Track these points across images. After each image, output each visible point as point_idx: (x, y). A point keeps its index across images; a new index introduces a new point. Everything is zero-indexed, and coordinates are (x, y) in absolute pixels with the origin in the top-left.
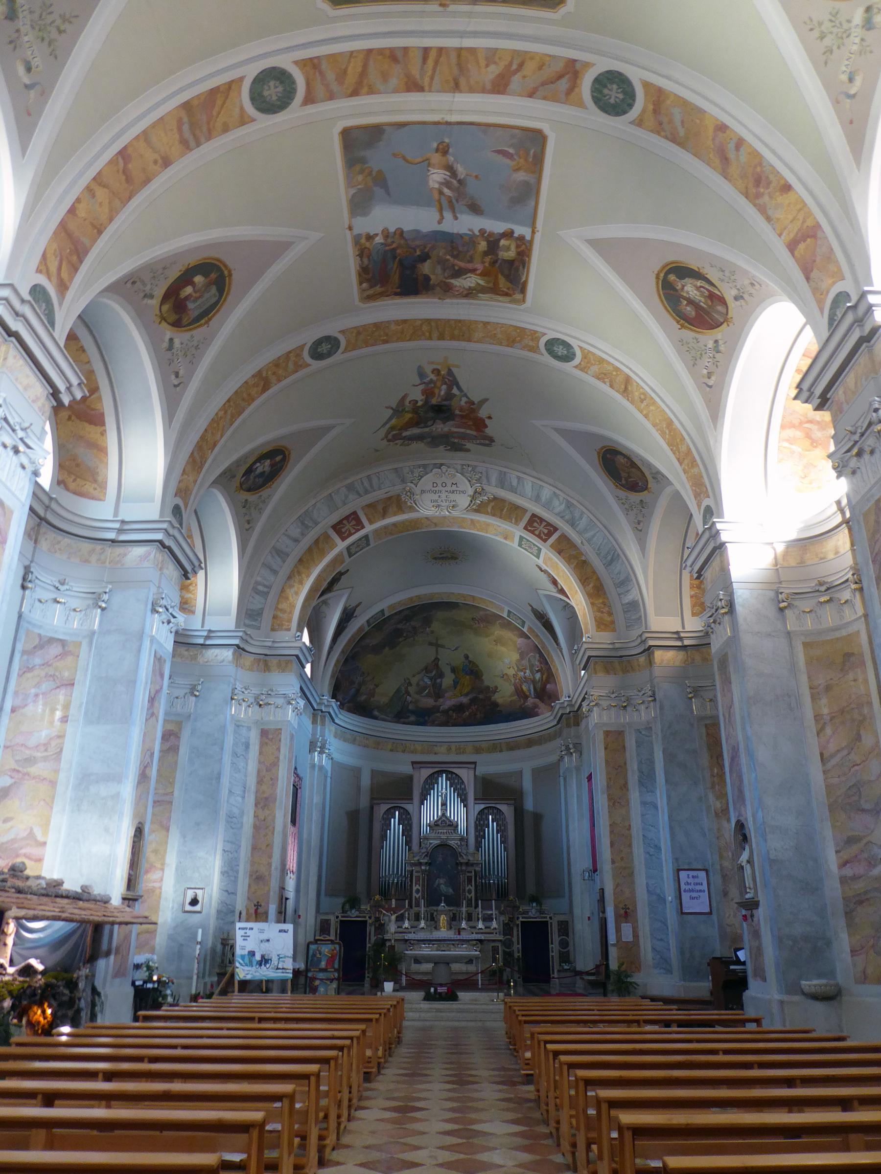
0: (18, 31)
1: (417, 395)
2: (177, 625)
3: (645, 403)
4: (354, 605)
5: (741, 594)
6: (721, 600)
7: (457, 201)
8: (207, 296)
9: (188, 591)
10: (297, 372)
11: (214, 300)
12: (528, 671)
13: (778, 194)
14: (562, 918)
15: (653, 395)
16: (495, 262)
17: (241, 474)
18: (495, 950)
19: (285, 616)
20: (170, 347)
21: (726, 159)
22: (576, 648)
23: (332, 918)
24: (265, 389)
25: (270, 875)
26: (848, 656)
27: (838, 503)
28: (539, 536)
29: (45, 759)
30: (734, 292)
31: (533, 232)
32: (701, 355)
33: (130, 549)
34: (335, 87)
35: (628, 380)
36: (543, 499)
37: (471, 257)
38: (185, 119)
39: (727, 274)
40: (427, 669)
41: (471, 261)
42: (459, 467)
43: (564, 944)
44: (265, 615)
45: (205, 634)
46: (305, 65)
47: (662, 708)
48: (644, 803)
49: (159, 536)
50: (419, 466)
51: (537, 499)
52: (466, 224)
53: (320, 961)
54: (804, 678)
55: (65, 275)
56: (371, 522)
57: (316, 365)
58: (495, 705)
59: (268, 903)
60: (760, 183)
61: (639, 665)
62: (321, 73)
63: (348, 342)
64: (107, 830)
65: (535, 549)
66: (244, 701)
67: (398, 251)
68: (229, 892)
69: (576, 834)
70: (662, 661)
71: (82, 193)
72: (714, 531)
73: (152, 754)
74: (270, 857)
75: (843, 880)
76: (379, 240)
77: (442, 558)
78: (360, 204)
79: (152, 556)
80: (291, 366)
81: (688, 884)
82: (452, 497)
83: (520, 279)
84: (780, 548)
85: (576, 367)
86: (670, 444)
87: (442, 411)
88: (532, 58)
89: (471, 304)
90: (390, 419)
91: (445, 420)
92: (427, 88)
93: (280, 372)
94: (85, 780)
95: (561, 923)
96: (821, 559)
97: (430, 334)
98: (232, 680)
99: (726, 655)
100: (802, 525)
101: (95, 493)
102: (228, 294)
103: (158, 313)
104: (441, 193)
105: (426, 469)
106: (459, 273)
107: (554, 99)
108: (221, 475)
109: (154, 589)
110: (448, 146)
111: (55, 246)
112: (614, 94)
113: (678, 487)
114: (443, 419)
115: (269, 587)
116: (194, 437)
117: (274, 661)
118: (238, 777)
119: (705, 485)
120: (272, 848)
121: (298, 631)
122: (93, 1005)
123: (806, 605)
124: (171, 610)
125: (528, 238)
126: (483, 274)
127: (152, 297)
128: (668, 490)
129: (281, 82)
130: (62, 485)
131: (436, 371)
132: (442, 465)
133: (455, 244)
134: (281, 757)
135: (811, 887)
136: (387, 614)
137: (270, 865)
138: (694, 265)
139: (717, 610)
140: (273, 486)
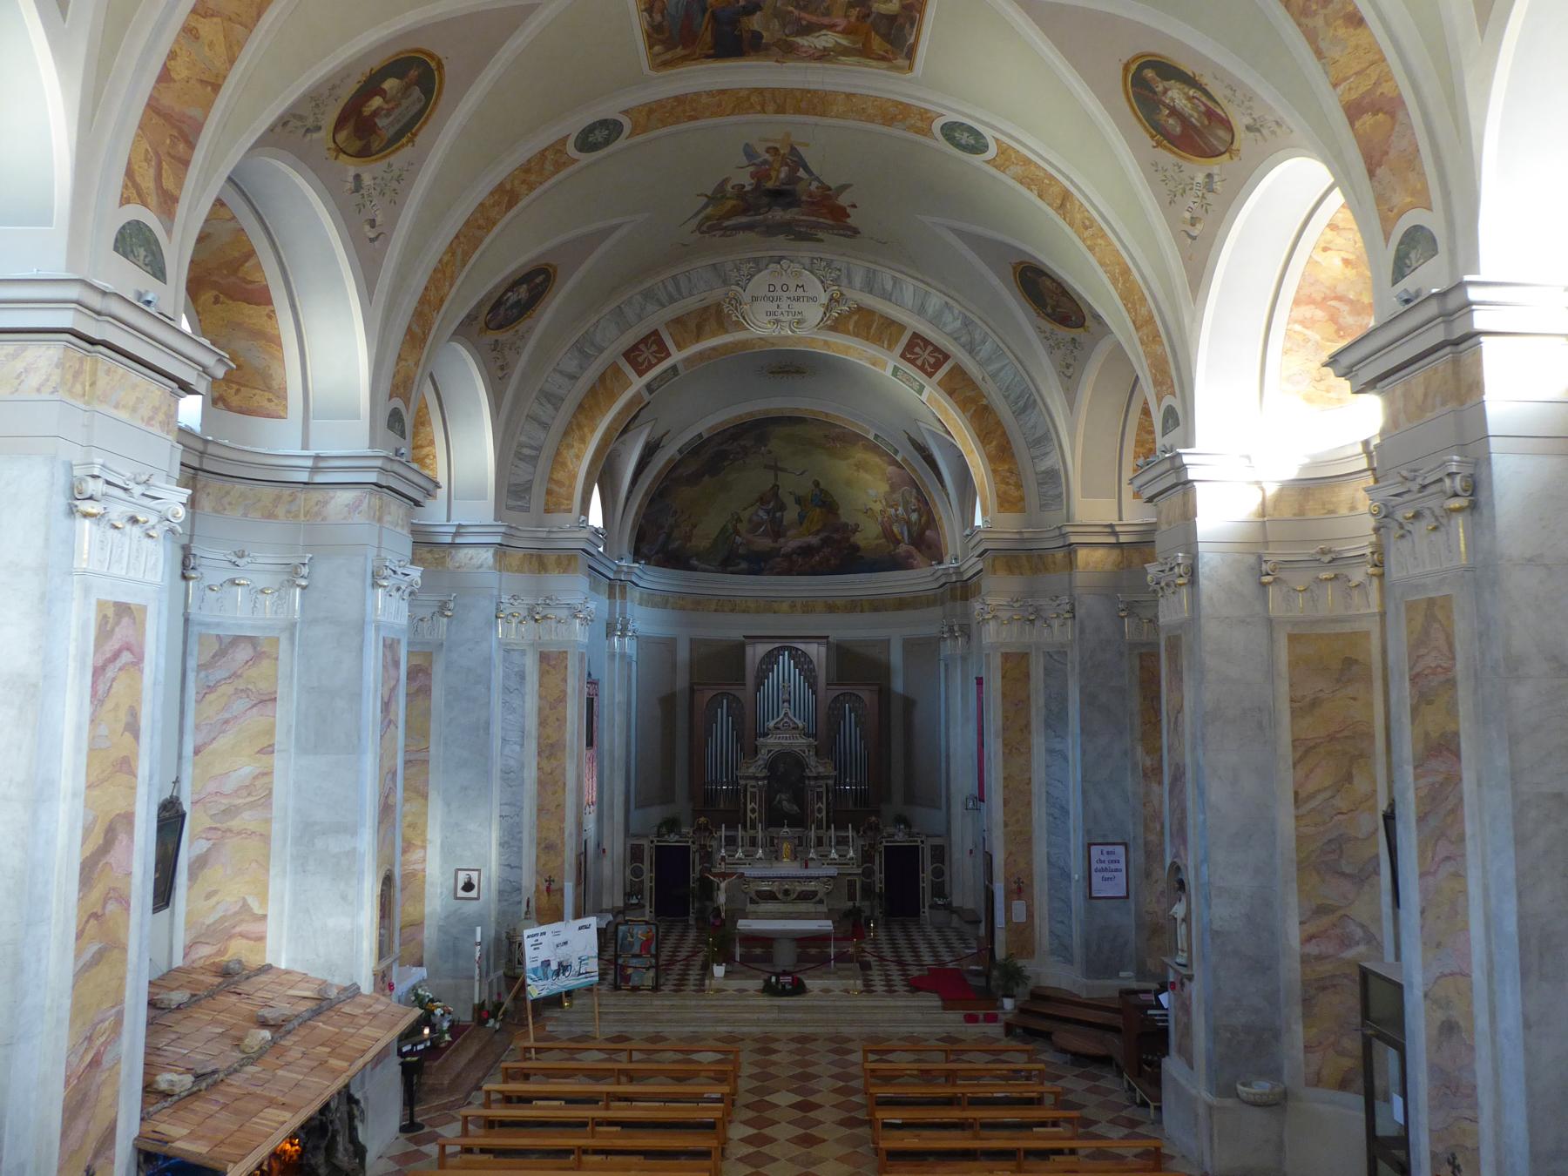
1: (747, 182)
5: (1210, 560)
8: (405, 103)
11: (418, 107)
13: (1340, 22)
14: (937, 841)
17: (482, 313)
18: (851, 884)
19: (563, 491)
23: (645, 843)
25: (563, 844)
26: (1349, 662)
27: (1366, 443)
28: (922, 368)
29: (252, 805)
30: (1247, 120)
33: (331, 493)
35: (1066, 196)
36: (930, 311)
40: (762, 500)
41: (827, 13)
42: (807, 262)
43: (939, 873)
44: (535, 489)
47: (1082, 631)
48: (1050, 751)
51: (921, 311)
53: (631, 945)
54: (1284, 688)
55: (168, 183)
56: (679, 347)
57: (586, 158)
58: (856, 548)
59: (562, 878)
64: (344, 897)
68: (511, 866)
69: (959, 740)
70: (1087, 564)
71: (177, 41)
73: (394, 774)
74: (562, 820)
75: (1305, 959)
79: (365, 506)
80: (549, 167)
81: (1101, 861)
82: (797, 306)
84: (1272, 490)
87: (782, 196)
90: (705, 207)
93: (533, 178)
94: (308, 832)
95: (934, 848)
96: (1331, 512)
100: (1307, 461)
101: (271, 407)
103: (332, 145)
105: (758, 265)
106: (809, 29)
111: (145, 145)
114: (784, 205)
115: (539, 449)
118: (511, 722)
120: (563, 810)
122: (351, 1117)
123: (1299, 580)
126: (846, 32)
127: (319, 128)
130: (220, 405)
132: (782, 258)
134: (569, 691)
135: (1262, 965)
136: (705, 436)
137: (562, 830)
138: (1187, 67)
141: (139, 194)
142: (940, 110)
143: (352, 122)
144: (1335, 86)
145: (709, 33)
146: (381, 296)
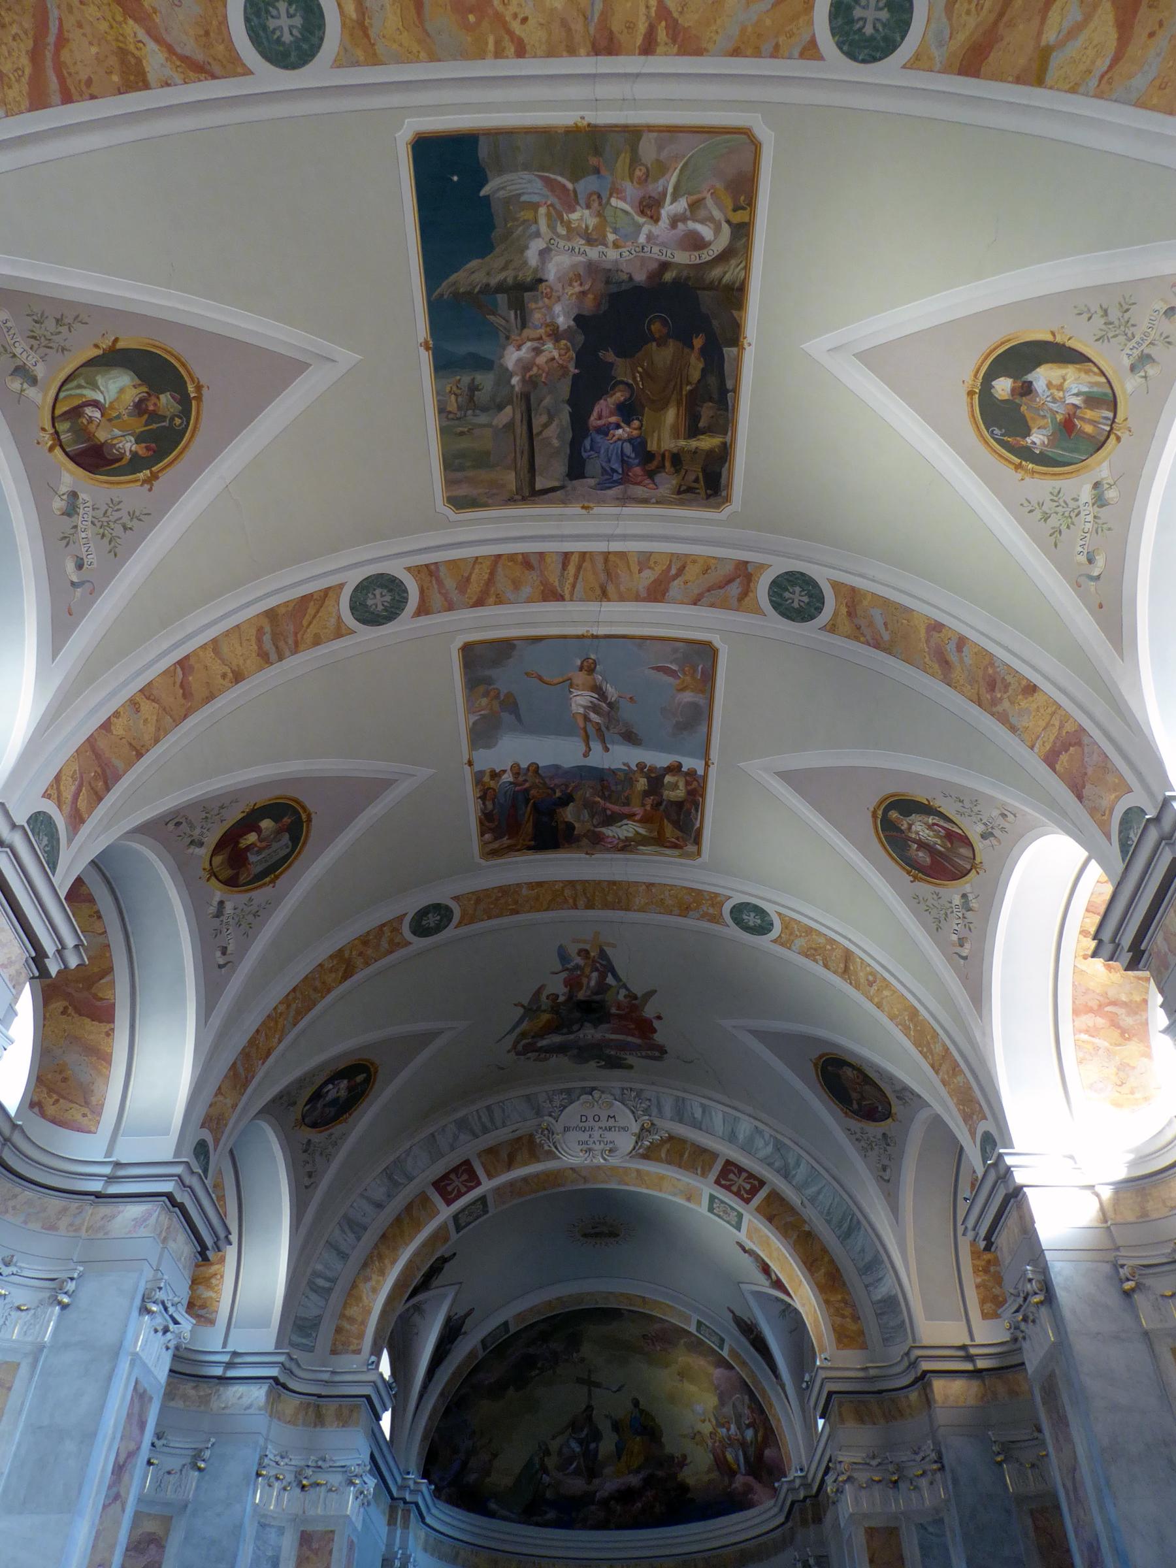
0: (75, 527)
1: (557, 987)
2: (179, 1336)
3: (875, 987)
4: (462, 1313)
5: (1061, 1270)
6: (1030, 1280)
7: (607, 728)
8: (275, 846)
9: (209, 1287)
10: (391, 952)
11: (282, 853)
12: (733, 1427)
13: (1020, 697)
15: (886, 975)
16: (660, 804)
17: (304, 1098)
19: (354, 1328)
20: (219, 913)
21: (947, 662)
22: (807, 1378)
24: (347, 975)
28: (737, 1194)
30: (980, 828)
31: (707, 765)
32: (946, 914)
33: (121, 1207)
34: (455, 596)
35: (848, 956)
36: (741, 1137)
37: (627, 798)
38: (268, 629)
39: (967, 804)
40: (574, 1426)
42: (618, 1092)
45: (226, 1358)
46: (419, 572)
47: (955, 1481)
49: (167, 1187)
50: (561, 1091)
51: (732, 1138)
52: (619, 757)
55: (82, 804)
56: (490, 1176)
57: (420, 943)
58: (684, 1488)
60: (994, 686)
61: (909, 1406)
62: (440, 583)
63: (464, 914)
65: (733, 1216)
66: (277, 1479)
67: (533, 792)
70: (946, 1397)
72: (1002, 1171)
76: (507, 777)
77: (597, 1235)
78: (483, 733)
79: (152, 1220)
80: (385, 944)
82: (609, 1136)
83: (693, 825)
84: (1107, 1193)
85: (775, 941)
86: (917, 1044)
87: (590, 1009)
88: (694, 562)
89: (628, 860)
91: (596, 1023)
92: (567, 596)
93: (369, 952)
97: (575, 901)
98: (261, 1441)
99: (1052, 1375)
100: (1131, 1156)
101: (85, 1122)
102: (305, 843)
103: (207, 866)
104: (586, 718)
105: (571, 1096)
106: (612, 819)
107: (724, 605)
108: (273, 1101)
109: (149, 1273)
110: (595, 662)
112: (797, 598)
113: (938, 1109)
114: (594, 1023)
115: (333, 1281)
116: (239, 1040)
117: (331, 1407)
119: (979, 1101)
121: (372, 1354)
124: (171, 1310)
125: (700, 772)
126: (645, 820)
127: (201, 844)
128: (923, 1115)
129: (390, 591)
130: (36, 1110)
131: (584, 953)
132: (594, 1089)
133: (602, 780)
136: (513, 1330)
138: (921, 796)
139: (1025, 1299)
140: (350, 1120)
141: (58, 797)
142: (729, 893)
143: (229, 849)
144: (1032, 748)
145: (531, 823)
146: (216, 1020)
